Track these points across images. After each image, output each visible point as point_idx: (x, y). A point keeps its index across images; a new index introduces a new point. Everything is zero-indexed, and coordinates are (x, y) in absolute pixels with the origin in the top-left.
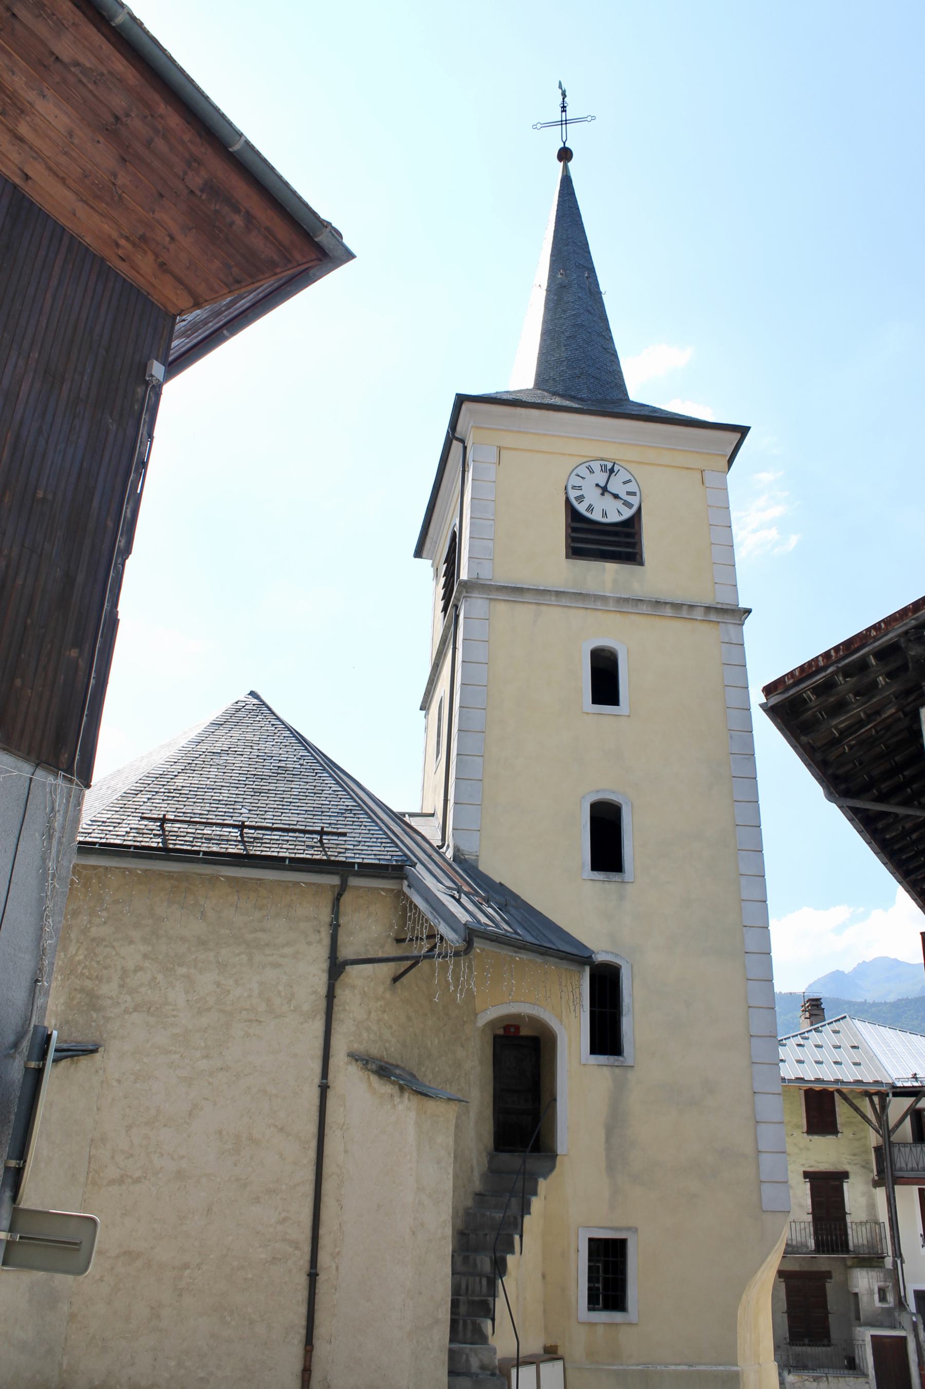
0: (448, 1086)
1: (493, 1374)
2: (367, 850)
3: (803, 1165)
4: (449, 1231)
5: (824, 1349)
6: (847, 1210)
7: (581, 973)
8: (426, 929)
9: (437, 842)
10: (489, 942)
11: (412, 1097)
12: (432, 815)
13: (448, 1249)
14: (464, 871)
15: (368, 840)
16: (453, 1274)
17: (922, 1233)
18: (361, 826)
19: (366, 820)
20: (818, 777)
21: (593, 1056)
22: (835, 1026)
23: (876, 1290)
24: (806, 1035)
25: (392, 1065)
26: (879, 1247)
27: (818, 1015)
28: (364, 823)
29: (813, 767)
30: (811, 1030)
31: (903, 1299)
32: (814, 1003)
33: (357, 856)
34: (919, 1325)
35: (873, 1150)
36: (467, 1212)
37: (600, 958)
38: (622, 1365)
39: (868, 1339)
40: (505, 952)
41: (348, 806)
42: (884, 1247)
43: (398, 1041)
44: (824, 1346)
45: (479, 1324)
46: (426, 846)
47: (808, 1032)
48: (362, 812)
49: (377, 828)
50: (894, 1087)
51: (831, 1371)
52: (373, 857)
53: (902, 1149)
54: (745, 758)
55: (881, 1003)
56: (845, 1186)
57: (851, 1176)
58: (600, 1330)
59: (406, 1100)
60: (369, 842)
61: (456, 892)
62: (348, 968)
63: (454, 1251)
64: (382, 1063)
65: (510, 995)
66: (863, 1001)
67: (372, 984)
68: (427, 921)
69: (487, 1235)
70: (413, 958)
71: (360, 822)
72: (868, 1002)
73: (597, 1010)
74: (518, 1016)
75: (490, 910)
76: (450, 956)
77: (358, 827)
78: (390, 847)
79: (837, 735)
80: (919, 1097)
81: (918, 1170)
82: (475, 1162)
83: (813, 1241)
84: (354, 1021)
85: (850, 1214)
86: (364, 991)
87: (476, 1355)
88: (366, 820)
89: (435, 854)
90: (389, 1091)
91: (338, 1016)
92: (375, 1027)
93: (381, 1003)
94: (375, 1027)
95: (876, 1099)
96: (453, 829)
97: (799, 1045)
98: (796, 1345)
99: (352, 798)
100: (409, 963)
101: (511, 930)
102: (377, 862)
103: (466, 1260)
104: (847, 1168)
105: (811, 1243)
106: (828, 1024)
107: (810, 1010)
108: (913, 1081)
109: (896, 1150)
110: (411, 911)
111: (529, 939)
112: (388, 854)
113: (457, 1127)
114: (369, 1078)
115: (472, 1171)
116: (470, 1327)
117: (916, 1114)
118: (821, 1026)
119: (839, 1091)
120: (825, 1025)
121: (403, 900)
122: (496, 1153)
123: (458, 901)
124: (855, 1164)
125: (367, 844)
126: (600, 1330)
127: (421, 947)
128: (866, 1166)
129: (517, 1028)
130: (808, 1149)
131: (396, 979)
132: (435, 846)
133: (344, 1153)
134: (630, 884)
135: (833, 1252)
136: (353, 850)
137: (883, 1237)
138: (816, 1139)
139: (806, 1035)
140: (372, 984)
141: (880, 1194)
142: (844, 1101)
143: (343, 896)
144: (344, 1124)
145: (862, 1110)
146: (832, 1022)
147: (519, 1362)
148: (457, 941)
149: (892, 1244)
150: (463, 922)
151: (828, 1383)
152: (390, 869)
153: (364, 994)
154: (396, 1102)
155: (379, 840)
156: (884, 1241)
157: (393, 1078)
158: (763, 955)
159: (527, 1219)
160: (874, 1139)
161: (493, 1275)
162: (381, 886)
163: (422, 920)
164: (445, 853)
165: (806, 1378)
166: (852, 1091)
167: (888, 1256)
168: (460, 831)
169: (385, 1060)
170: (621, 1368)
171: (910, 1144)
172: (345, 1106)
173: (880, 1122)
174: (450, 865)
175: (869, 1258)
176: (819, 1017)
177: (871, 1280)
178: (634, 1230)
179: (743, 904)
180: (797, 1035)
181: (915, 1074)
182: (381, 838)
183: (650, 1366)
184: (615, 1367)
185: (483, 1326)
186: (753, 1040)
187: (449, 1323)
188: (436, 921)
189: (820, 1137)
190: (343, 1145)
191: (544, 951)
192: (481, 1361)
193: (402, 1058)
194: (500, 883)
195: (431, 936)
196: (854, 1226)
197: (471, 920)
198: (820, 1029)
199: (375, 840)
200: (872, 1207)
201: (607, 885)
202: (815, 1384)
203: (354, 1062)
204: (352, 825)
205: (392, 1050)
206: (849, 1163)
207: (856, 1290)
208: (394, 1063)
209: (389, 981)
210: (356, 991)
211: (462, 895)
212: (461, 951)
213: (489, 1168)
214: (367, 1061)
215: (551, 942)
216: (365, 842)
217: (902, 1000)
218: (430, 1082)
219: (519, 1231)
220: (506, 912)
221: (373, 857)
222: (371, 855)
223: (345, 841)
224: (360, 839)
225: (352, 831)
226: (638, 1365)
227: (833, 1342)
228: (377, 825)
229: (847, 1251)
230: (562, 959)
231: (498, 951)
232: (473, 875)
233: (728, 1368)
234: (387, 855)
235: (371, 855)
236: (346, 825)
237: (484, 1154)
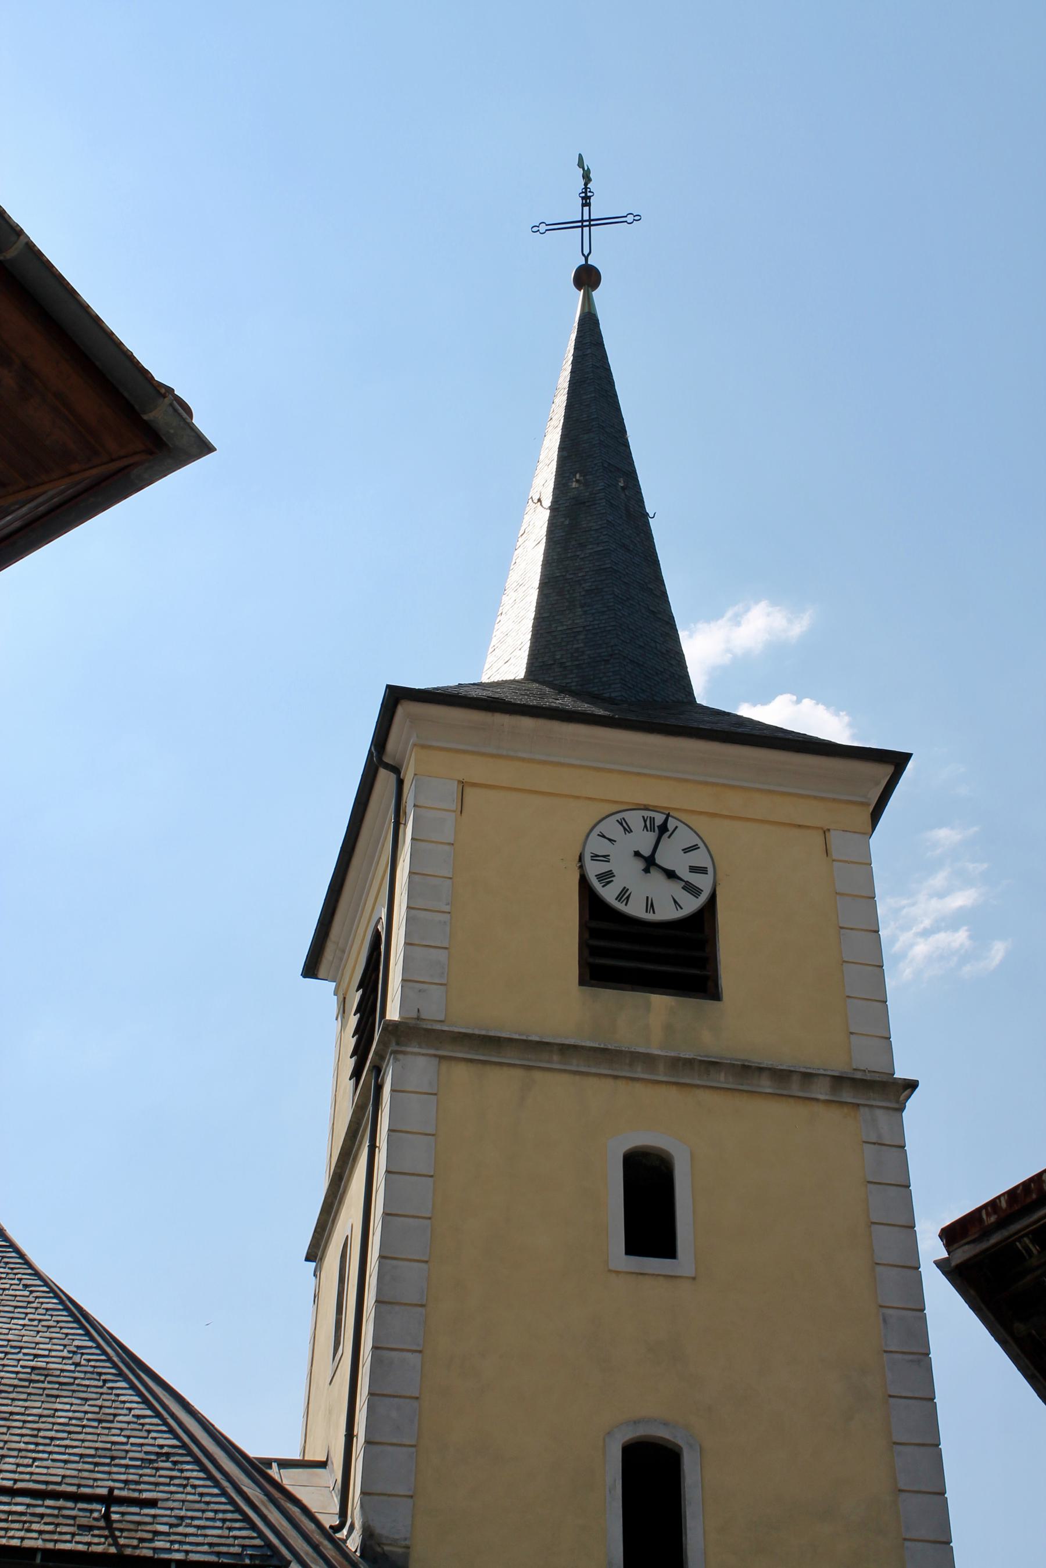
12: (323, 1465)
15: (199, 1514)
18: (185, 1486)
19: (195, 1474)
41: (161, 1446)
46: (309, 1526)
48: (188, 1459)
77: (181, 1489)
78: (240, 1529)
88: (195, 1474)
89: (326, 1543)
102: (213, 1558)
125: (196, 1522)
136: (168, 1534)
155: (220, 1516)
164: (345, 1541)
204: (169, 1485)
216: (192, 1518)
221: (206, 1548)
222: (202, 1544)
224: (183, 1513)
225: (169, 1496)
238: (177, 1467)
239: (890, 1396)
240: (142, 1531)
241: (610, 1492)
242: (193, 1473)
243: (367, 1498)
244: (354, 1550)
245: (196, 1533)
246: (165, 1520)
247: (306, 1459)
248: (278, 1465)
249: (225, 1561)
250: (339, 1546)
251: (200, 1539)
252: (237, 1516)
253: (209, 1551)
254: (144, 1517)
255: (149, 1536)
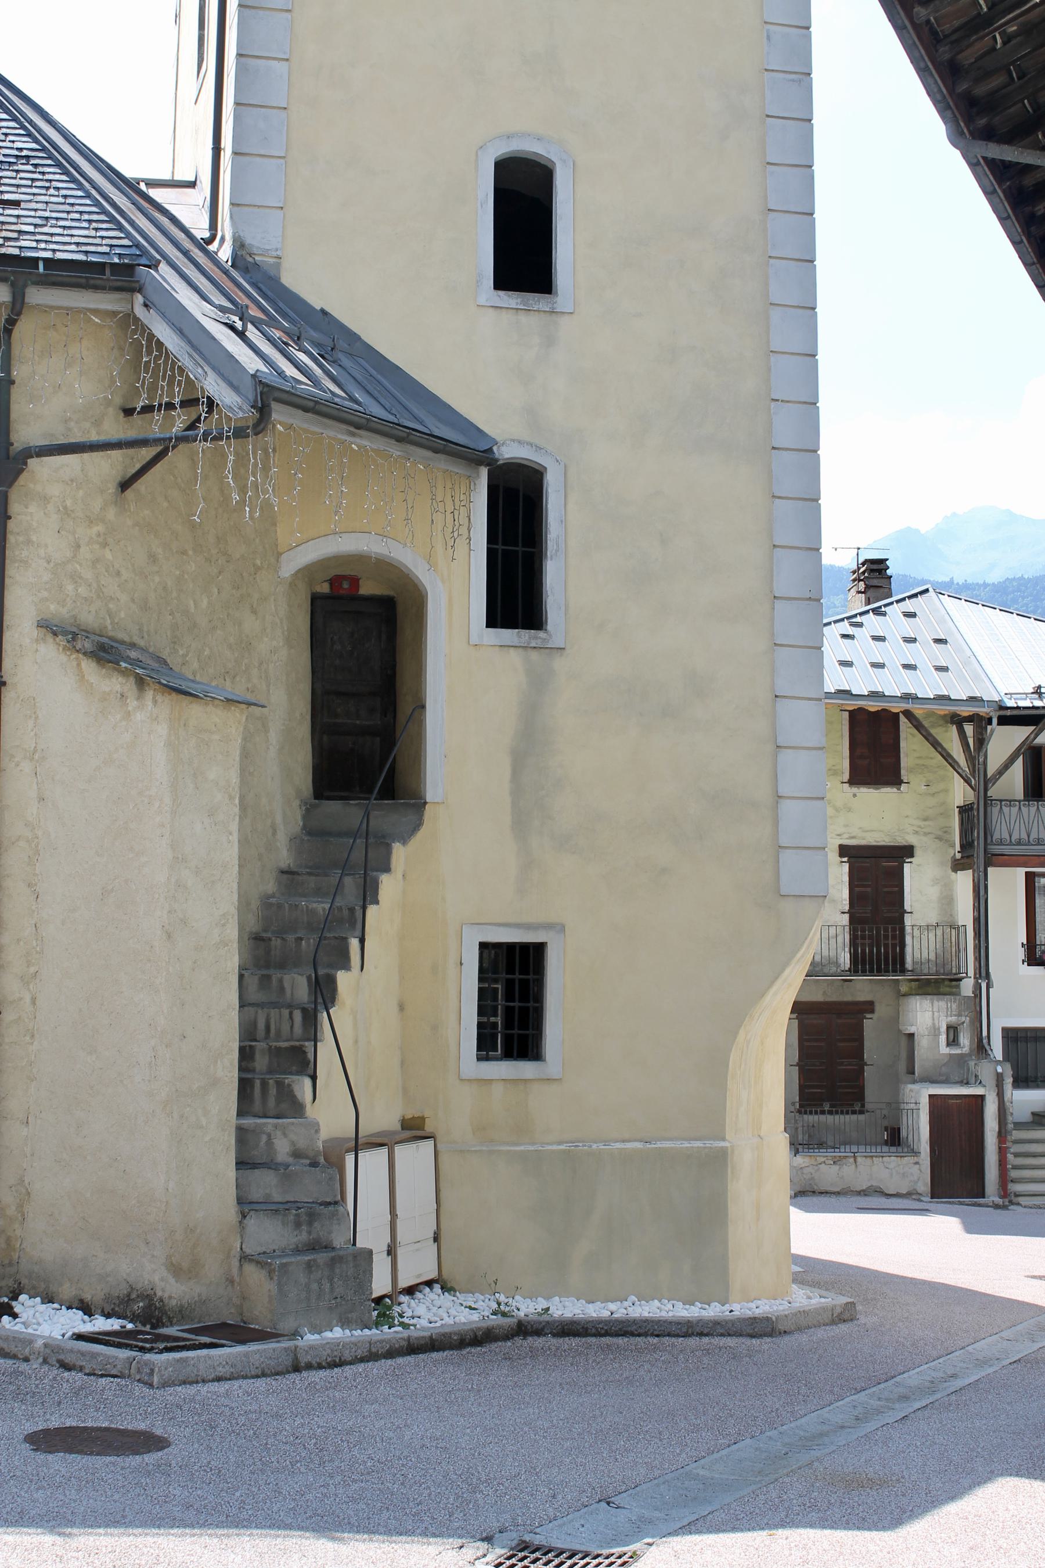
0: (228, 683)
1: (314, 1164)
2: (62, 235)
3: (838, 835)
4: (232, 932)
5: (854, 1117)
6: (907, 907)
7: (471, 479)
8: (179, 384)
9: (202, 232)
10: (300, 412)
11: (159, 698)
12: (192, 185)
13: (232, 962)
14: (254, 285)
15: (64, 215)
16: (242, 1006)
17: (1025, 943)
18: (48, 188)
19: (57, 177)
20: (939, 97)
21: (491, 631)
22: (909, 606)
23: (944, 1029)
24: (858, 619)
25: (122, 642)
26: (954, 963)
27: (881, 587)
28: (55, 184)
29: (932, 75)
30: (867, 612)
31: (985, 1041)
32: (875, 567)
33: (43, 245)
34: (1005, 1078)
35: (957, 810)
36: (266, 903)
37: (507, 453)
38: (533, 1144)
39: (925, 1102)
40: (332, 434)
41: (21, 149)
42: (962, 964)
43: (133, 600)
44: (854, 1112)
45: (289, 1085)
46: (180, 236)
47: (862, 614)
48: (50, 162)
49: (80, 193)
50: (1002, 708)
51: (862, 1148)
52: (73, 247)
53: (1006, 810)
54: (793, 81)
55: (977, 584)
56: (907, 868)
57: (917, 852)
58: (498, 1090)
59: (149, 703)
60: (66, 219)
61: (236, 319)
62: (32, 462)
63: (242, 968)
64: (104, 640)
65: (336, 513)
66: (947, 579)
67: (81, 493)
68: (181, 370)
69: (301, 939)
70: (157, 441)
71: (47, 180)
72: (955, 582)
73: (500, 547)
74: (360, 559)
75: (302, 357)
76: (228, 437)
77: (43, 191)
78: (107, 229)
79: (985, 10)
80: (1040, 726)
81: (1029, 843)
82: (279, 819)
83: (848, 956)
84: (49, 562)
85: (911, 913)
86: (65, 508)
87: (285, 1135)
88: (57, 177)
89: (196, 251)
90: (118, 688)
91: (17, 553)
92: (88, 574)
93: (100, 528)
94: (88, 574)
95: (969, 729)
96: (232, 204)
97: (845, 636)
98: (811, 1113)
99: (29, 135)
100: (147, 454)
101: (343, 395)
102: (81, 257)
103: (265, 981)
104: (911, 839)
105: (845, 959)
106: (898, 601)
107: (865, 578)
108: (1035, 699)
109: (995, 810)
110: (149, 353)
111: (377, 410)
112: (104, 242)
113: (245, 755)
114: (79, 665)
115: (274, 833)
116: (273, 1091)
117: (1033, 755)
118: (885, 606)
119: (908, 714)
120: (892, 603)
121: (135, 332)
122: (317, 801)
123: (241, 335)
124: (926, 834)
125: (61, 223)
126: (498, 1090)
127: (170, 421)
128: (942, 838)
129: (355, 581)
130: (850, 810)
131: (125, 485)
132: (199, 237)
133: (39, 802)
134: (566, 317)
135: (879, 972)
136: (33, 233)
137: (962, 947)
138: (866, 793)
139: (858, 619)
140: (81, 493)
141: (964, 881)
142: (915, 731)
143: (18, 323)
144: (35, 750)
145: (945, 745)
146: (903, 599)
147: (357, 1146)
148: (240, 408)
149: (975, 958)
150: (252, 372)
151: (856, 1166)
152: (108, 271)
153: (66, 512)
154: (130, 708)
155: (86, 217)
156: (962, 954)
157: (123, 664)
158: (802, 453)
159: (372, 911)
160: (960, 793)
161: (313, 1006)
162: (92, 306)
163: (172, 369)
164: (216, 253)
165: (823, 1159)
166: (931, 714)
167: (967, 977)
168: (246, 209)
169: (111, 634)
170: (531, 1148)
171: (1019, 801)
172: (37, 718)
173: (974, 766)
174: (226, 272)
175: (936, 981)
176: (882, 590)
177: (936, 1014)
178: (560, 928)
179: (773, 358)
180: (842, 620)
181: (1039, 687)
182: (90, 213)
183: (581, 1144)
184: (522, 1148)
185: (296, 1089)
186: (778, 604)
187: (237, 1085)
188: (200, 370)
189: (871, 790)
190: (35, 787)
191: (405, 435)
192: (293, 1143)
193: (141, 630)
194: (323, 312)
195: (189, 403)
196: (916, 933)
197: (266, 370)
198: (883, 609)
199: (77, 216)
200: (948, 901)
201: (523, 318)
202: (836, 1168)
203: (50, 638)
204: (31, 187)
205: (123, 615)
206: (916, 833)
207: (912, 1030)
208: (127, 639)
209: (112, 488)
210: (50, 507)
211: (250, 326)
212: (248, 428)
213: (304, 827)
214: (75, 636)
215: (416, 419)
216: (57, 219)
217: (1014, 579)
218: (194, 674)
219: (358, 933)
220: (334, 362)
221: (73, 247)
222: (70, 244)
223: (18, 217)
224: (47, 214)
225: (31, 197)
226: (560, 1143)
227: (868, 1106)
228: (81, 187)
229: (903, 970)
230: (436, 451)
231: (317, 429)
232: (269, 293)
233: (709, 1144)
234: (101, 245)
235: (70, 244)
236: (18, 186)
237: (296, 803)
238: (38, 170)
239: (768, 116)
240: (6, 230)
241: (482, 206)
242: (54, 174)
243: (236, 209)
244: (226, 260)
245: (62, 233)
246: (29, 220)
247: (175, 179)
248: (146, 184)
249: (93, 259)
250: (212, 257)
251: (67, 239)
252: (103, 217)
253: (77, 250)
254: (7, 217)
255: (15, 235)
